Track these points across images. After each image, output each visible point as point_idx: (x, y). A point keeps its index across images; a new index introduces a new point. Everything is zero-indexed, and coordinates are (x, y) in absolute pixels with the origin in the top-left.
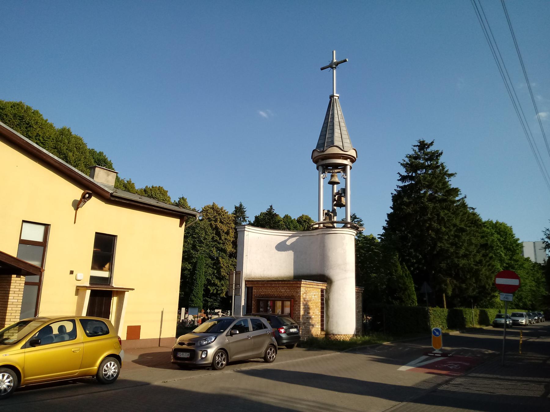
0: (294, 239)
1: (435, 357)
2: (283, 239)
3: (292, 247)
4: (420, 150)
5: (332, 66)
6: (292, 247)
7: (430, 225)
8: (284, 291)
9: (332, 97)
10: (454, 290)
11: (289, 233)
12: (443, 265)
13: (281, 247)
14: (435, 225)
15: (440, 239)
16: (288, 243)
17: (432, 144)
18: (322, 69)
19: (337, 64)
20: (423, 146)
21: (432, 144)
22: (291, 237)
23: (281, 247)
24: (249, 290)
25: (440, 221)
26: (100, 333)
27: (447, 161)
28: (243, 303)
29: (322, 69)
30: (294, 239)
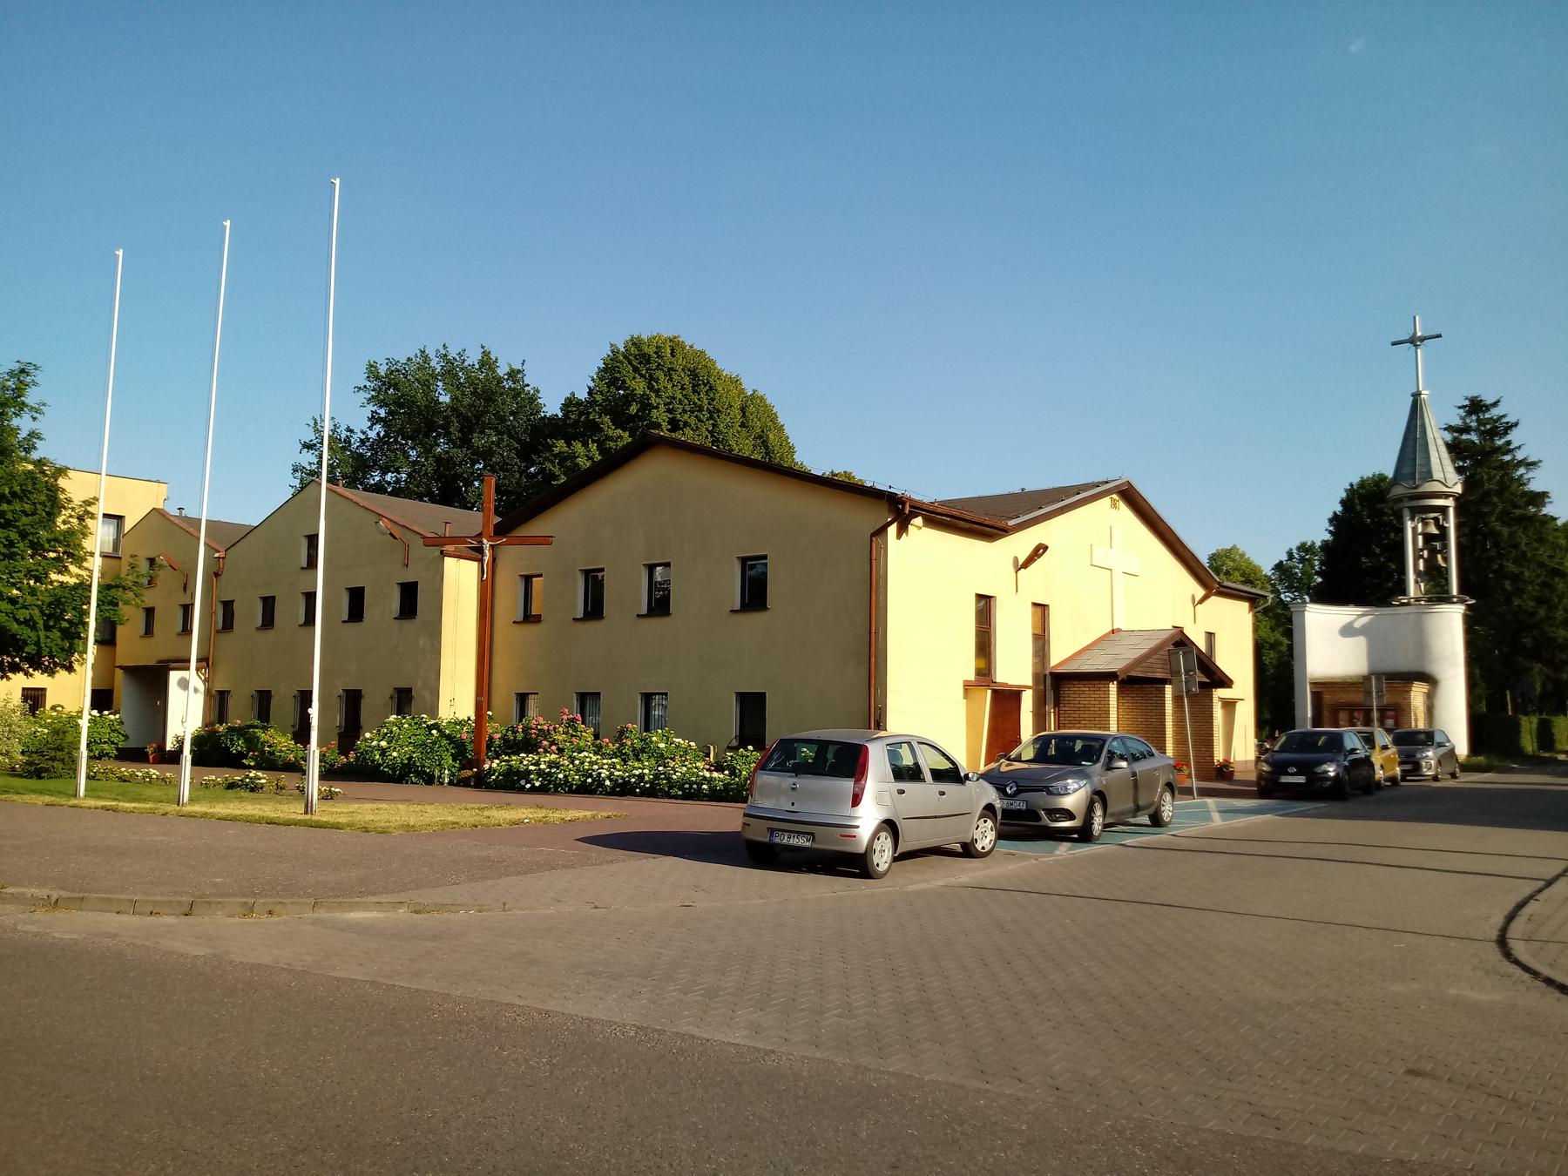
0: (1365, 620)
1: (1018, 759)
2: (1348, 619)
3: (1362, 631)
4: (1469, 413)
5: (1414, 341)
6: (1362, 631)
7: (1502, 566)
8: (1357, 697)
9: (1416, 396)
10: (1544, 686)
11: (1359, 610)
12: (1527, 641)
13: (1348, 631)
14: (1511, 567)
15: (1519, 592)
16: (1357, 625)
17: (1495, 404)
18: (1394, 344)
19: (1423, 339)
20: (1476, 406)
21: (1495, 404)
22: (1360, 616)
23: (1348, 631)
24: (1317, 697)
25: (1522, 559)
26: (433, 677)
27: (1524, 442)
28: (1309, 715)
29: (1394, 344)
30: (1365, 620)
